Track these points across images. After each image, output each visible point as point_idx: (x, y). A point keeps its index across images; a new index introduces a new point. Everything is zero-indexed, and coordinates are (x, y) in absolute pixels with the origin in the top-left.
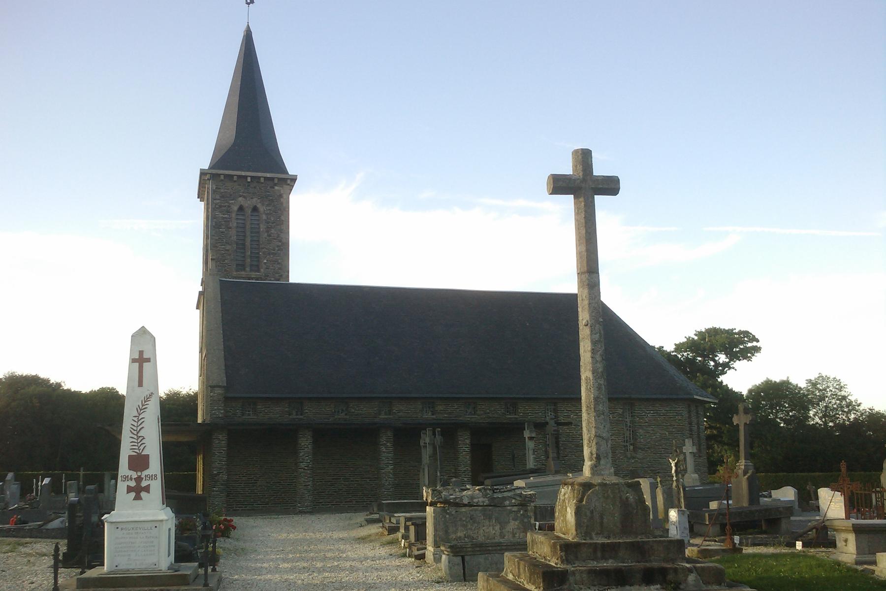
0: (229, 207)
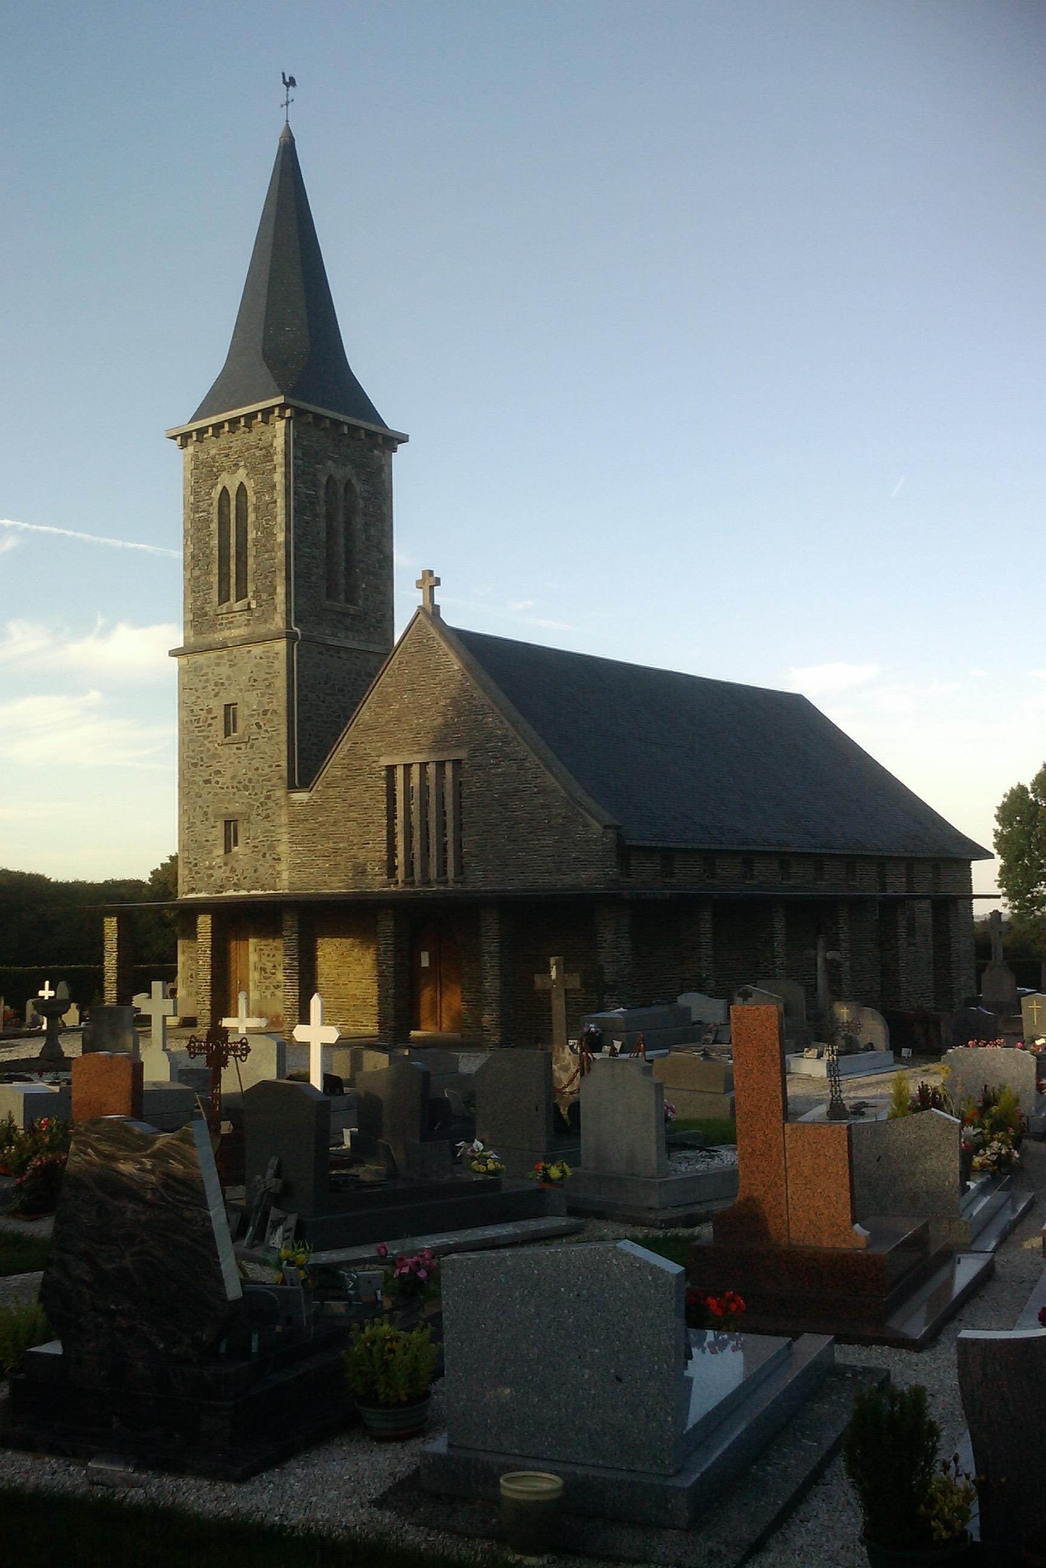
0: (314, 475)
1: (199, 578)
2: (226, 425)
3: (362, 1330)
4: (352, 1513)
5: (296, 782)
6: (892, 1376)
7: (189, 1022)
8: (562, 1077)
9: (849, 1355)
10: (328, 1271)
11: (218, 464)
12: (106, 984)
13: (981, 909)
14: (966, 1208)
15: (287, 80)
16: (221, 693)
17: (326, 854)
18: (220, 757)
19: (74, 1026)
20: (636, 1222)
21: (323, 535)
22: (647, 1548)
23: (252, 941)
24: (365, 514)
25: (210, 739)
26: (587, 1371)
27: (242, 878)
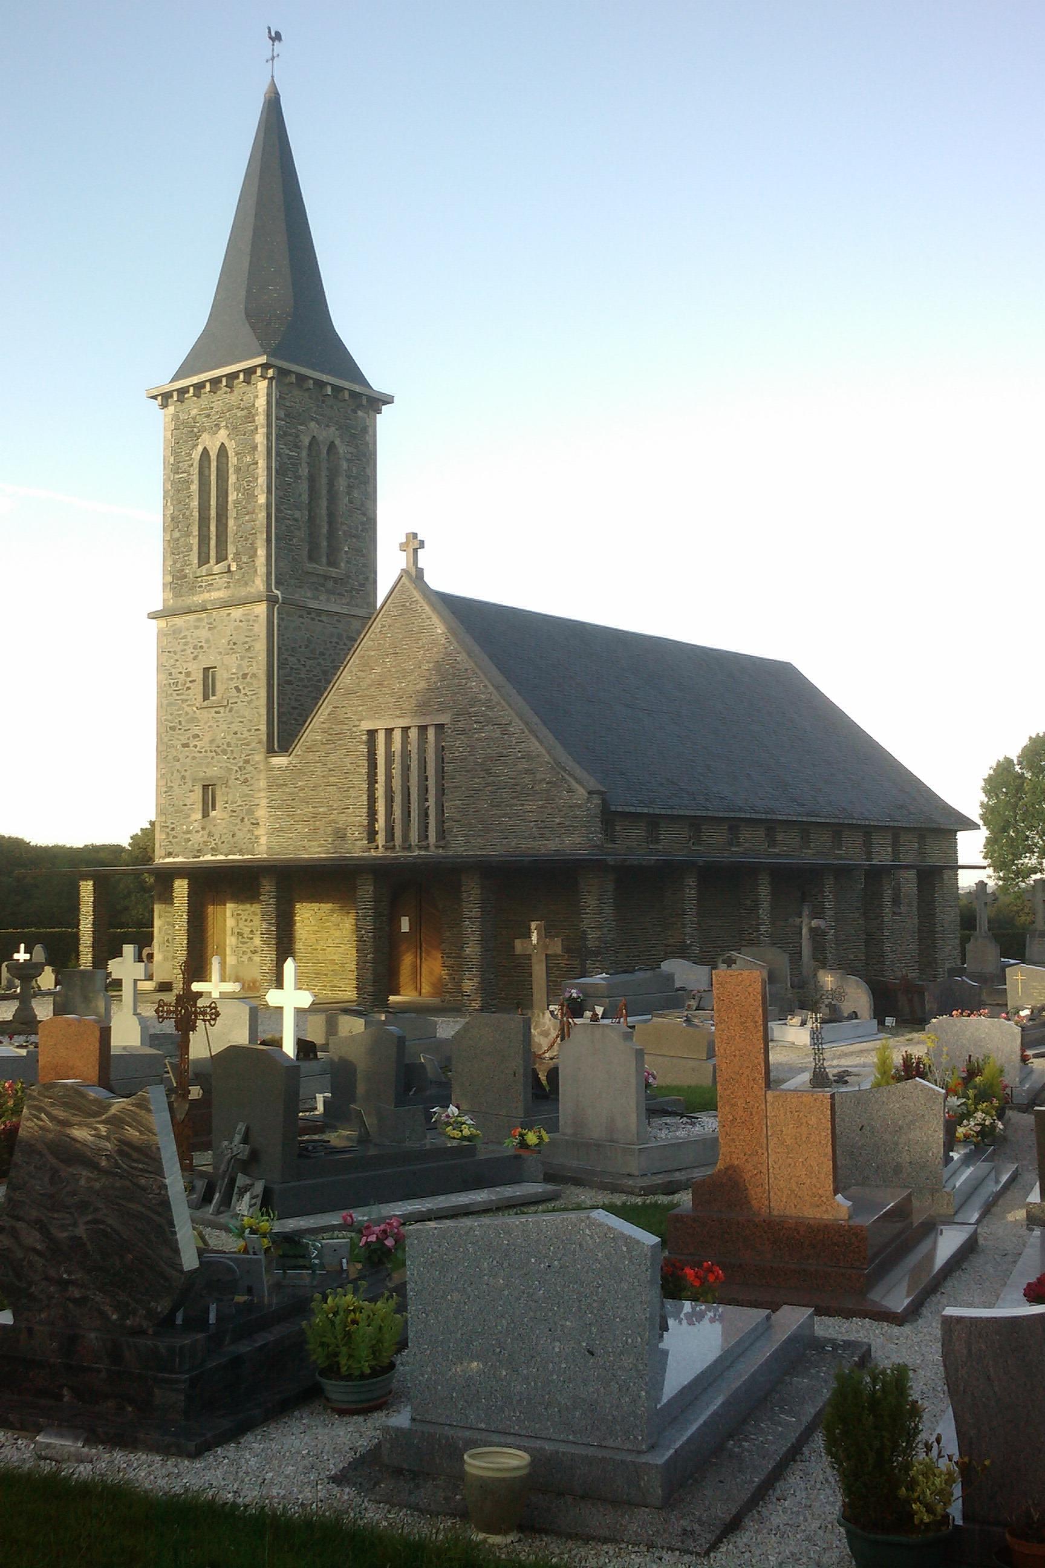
0: (297, 436)
1: (178, 540)
2: (208, 385)
3: (325, 1299)
4: (310, 1488)
5: (276, 746)
6: (873, 1349)
7: (165, 987)
8: (542, 1042)
9: (830, 1328)
10: (290, 1240)
11: (198, 424)
12: (81, 948)
13: (966, 880)
14: (949, 1179)
15: (273, 34)
16: (200, 657)
17: (305, 819)
18: (199, 721)
19: (49, 989)
20: (615, 1189)
21: (305, 497)
22: (618, 1526)
23: (230, 906)
24: (349, 477)
25: (189, 703)
26: (558, 1344)
27: (220, 843)
